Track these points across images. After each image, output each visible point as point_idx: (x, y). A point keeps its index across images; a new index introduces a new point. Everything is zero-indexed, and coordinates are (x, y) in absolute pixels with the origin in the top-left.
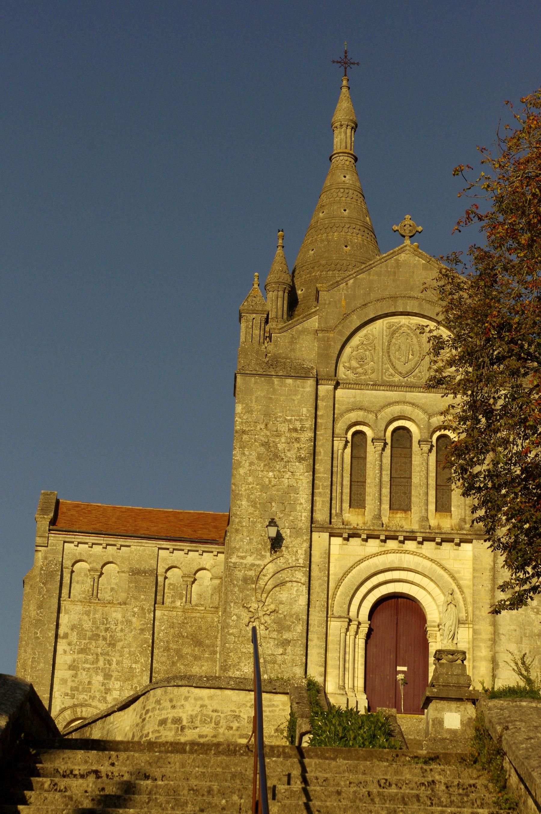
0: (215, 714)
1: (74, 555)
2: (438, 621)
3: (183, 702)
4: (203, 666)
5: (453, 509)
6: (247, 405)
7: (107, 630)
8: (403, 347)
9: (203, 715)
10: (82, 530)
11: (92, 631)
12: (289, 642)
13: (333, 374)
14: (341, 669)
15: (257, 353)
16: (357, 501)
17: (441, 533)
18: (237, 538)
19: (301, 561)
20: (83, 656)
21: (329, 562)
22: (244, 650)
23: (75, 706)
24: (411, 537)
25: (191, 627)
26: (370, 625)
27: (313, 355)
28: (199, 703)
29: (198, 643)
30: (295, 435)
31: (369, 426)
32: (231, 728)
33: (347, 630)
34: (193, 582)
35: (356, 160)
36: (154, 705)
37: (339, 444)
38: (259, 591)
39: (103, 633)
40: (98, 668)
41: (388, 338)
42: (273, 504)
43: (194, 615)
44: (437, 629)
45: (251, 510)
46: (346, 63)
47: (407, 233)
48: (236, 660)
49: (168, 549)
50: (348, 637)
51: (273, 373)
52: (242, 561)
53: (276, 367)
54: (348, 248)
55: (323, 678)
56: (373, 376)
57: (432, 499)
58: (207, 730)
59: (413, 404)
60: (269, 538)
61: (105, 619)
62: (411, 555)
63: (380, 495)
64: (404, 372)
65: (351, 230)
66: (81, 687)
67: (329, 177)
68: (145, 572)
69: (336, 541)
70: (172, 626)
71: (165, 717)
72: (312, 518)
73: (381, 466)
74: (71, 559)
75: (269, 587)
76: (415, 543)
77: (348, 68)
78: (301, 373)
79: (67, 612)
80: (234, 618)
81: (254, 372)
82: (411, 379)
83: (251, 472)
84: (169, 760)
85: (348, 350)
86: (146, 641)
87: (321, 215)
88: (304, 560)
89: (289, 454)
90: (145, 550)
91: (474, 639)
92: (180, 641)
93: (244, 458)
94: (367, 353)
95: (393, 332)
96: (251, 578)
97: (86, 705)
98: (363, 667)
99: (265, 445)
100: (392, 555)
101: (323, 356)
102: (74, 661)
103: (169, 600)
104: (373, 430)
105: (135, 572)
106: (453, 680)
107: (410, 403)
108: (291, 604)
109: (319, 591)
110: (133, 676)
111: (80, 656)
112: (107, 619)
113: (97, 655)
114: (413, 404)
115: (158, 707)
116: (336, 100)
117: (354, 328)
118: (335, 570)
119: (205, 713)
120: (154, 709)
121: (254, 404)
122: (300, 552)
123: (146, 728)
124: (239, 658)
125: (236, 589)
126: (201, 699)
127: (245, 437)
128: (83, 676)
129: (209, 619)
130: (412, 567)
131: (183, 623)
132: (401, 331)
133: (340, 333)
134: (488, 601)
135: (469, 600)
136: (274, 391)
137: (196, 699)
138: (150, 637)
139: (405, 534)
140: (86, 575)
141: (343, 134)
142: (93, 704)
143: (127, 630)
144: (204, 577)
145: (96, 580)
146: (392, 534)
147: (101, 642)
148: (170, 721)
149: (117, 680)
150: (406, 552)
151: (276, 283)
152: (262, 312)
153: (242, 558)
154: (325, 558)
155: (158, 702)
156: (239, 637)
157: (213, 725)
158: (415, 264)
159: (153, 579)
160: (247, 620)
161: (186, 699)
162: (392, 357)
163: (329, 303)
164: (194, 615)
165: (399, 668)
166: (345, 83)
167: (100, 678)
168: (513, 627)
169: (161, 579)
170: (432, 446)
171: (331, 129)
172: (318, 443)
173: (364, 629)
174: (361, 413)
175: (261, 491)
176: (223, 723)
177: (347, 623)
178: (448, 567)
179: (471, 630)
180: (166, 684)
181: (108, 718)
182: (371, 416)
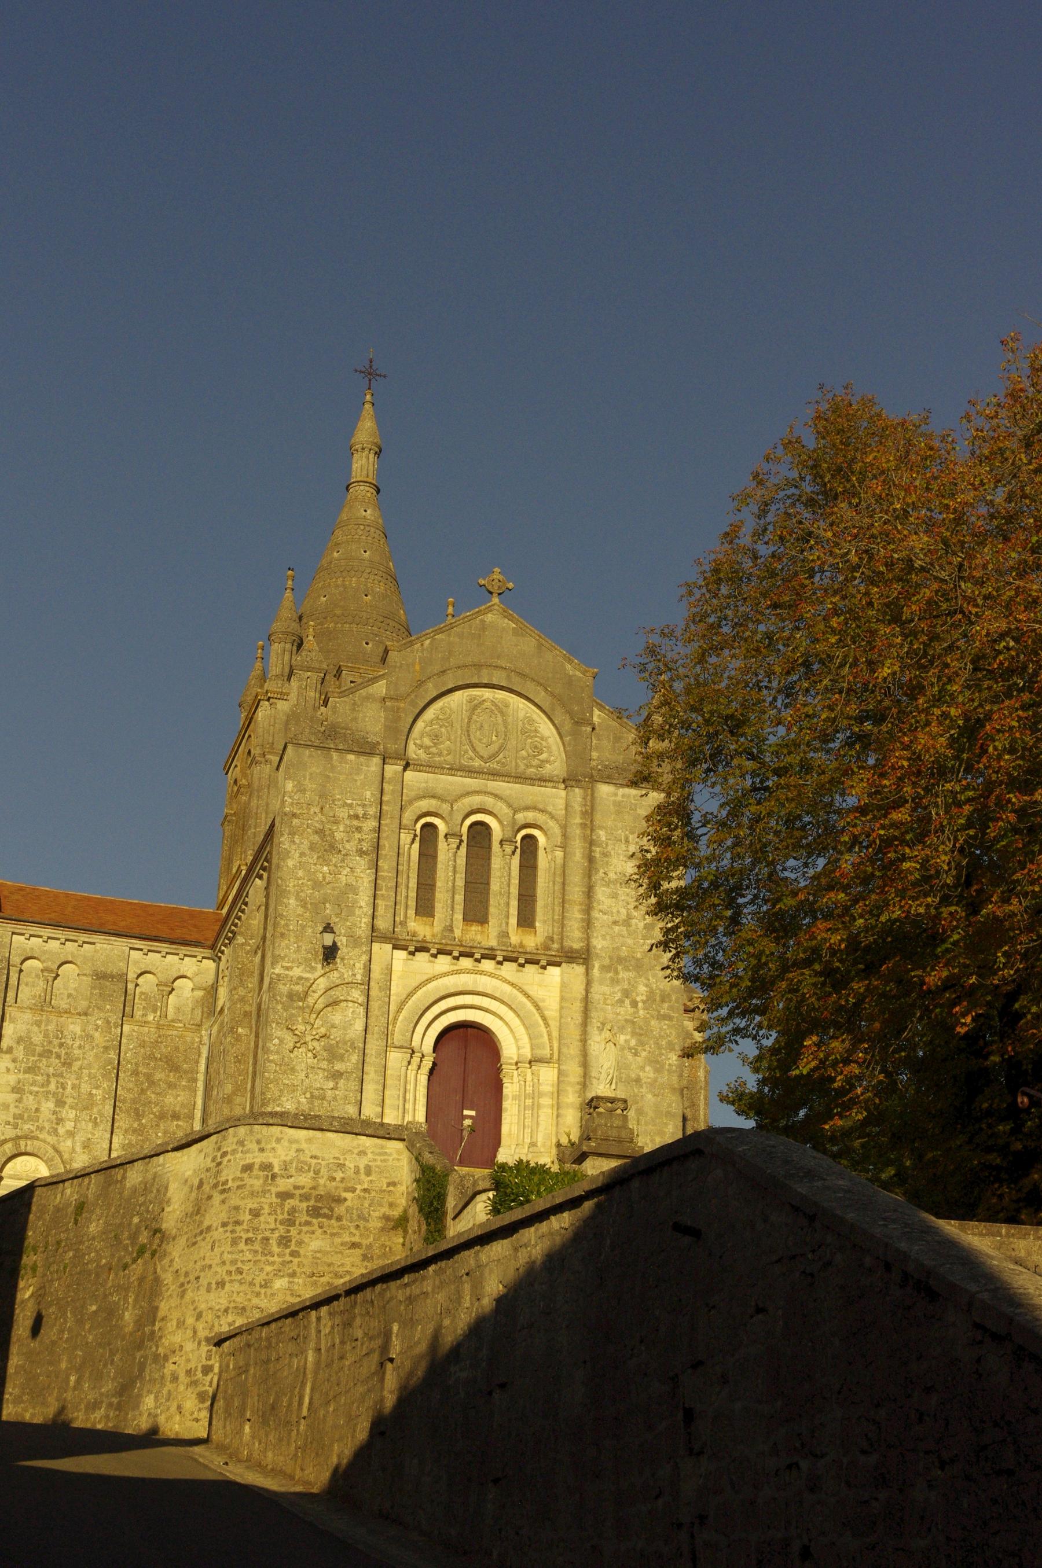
0: (314, 1161)
1: (25, 950)
2: (516, 1059)
3: (274, 1145)
4: (179, 1095)
5: (537, 924)
6: (299, 782)
7: (61, 1045)
8: (486, 727)
9: (299, 1161)
10: (35, 920)
11: (43, 1046)
12: (342, 1074)
14: (401, 1110)
15: (311, 720)
16: (425, 907)
17: (526, 953)
18: (283, 944)
19: (359, 977)
20: (31, 1076)
22: (287, 1082)
23: (18, 1137)
25: (166, 1047)
27: (378, 728)
28: (295, 1146)
29: (174, 1068)
30: (355, 823)
32: (334, 1179)
33: (409, 1063)
34: (170, 993)
35: (378, 491)
36: (234, 1147)
37: (406, 837)
38: (307, 1010)
39: (57, 1050)
40: (49, 1092)
41: (468, 714)
42: (328, 905)
43: (170, 1033)
44: (514, 1067)
45: (300, 911)
46: (370, 373)
47: (495, 589)
48: (277, 1094)
49: (141, 950)
50: (409, 1072)
51: (332, 746)
52: (287, 972)
53: (334, 739)
54: (369, 597)
56: (449, 758)
57: (514, 911)
58: (304, 1180)
59: (496, 796)
60: (323, 946)
61: (60, 1031)
62: (488, 977)
63: (453, 902)
65: (372, 577)
66: (26, 1115)
67: (346, 510)
68: (112, 977)
69: (400, 955)
70: (143, 1045)
71: (251, 1161)
73: (455, 867)
74: (20, 955)
76: (493, 962)
77: (373, 381)
78: (366, 749)
80: (276, 1041)
81: (309, 743)
82: (493, 765)
83: (301, 865)
84: (1012, 1246)
85: (420, 724)
87: (335, 554)
88: (363, 976)
89: (348, 846)
90: (113, 950)
91: (559, 1082)
92: (152, 1064)
93: (294, 847)
94: (443, 730)
95: (475, 706)
96: (298, 993)
97: (33, 1138)
98: (425, 1109)
99: (320, 832)
100: (465, 975)
101: (391, 729)
102: (19, 1082)
103: (140, 1013)
104: (447, 823)
105: (100, 976)
106: (613, 1133)
107: (492, 794)
108: (345, 1029)
109: (379, 1014)
110: (92, 1104)
111: (27, 1076)
112: (62, 1033)
113: (48, 1075)
114: (496, 796)
115: (241, 1149)
118: (397, 989)
119: (302, 1159)
120: (234, 1151)
121: (307, 782)
122: (357, 965)
123: (224, 1173)
125: (279, 1007)
126: (297, 1141)
127: (295, 821)
128: (30, 1101)
129: (188, 1039)
130: (489, 992)
131: (157, 1042)
132: (484, 707)
133: (413, 703)
134: (578, 1037)
136: (333, 767)
137: (291, 1142)
139: (483, 951)
140: (37, 976)
141: (364, 460)
142: (41, 1136)
143: (87, 1047)
145: (50, 983)
146: (468, 950)
147: (54, 1060)
148: (257, 1167)
149: (72, 1108)
150: (482, 973)
151: (283, 633)
152: (319, 670)
154: (386, 974)
155: (241, 1143)
156: (281, 1065)
157: (312, 1174)
158: (503, 628)
159: (122, 985)
160: (292, 1045)
161: (278, 1140)
162: (472, 737)
163: (401, 667)
164: (170, 1033)
165: (466, 1112)
166: (368, 397)
167: (51, 1105)
169: (131, 986)
170: (516, 847)
171: (350, 452)
172: (383, 835)
173: (428, 1064)
174: (434, 802)
175: (313, 889)
176: (324, 1172)
178: (531, 993)
179: (556, 1070)
180: (251, 1121)
181: (155, 1158)
182: (446, 807)
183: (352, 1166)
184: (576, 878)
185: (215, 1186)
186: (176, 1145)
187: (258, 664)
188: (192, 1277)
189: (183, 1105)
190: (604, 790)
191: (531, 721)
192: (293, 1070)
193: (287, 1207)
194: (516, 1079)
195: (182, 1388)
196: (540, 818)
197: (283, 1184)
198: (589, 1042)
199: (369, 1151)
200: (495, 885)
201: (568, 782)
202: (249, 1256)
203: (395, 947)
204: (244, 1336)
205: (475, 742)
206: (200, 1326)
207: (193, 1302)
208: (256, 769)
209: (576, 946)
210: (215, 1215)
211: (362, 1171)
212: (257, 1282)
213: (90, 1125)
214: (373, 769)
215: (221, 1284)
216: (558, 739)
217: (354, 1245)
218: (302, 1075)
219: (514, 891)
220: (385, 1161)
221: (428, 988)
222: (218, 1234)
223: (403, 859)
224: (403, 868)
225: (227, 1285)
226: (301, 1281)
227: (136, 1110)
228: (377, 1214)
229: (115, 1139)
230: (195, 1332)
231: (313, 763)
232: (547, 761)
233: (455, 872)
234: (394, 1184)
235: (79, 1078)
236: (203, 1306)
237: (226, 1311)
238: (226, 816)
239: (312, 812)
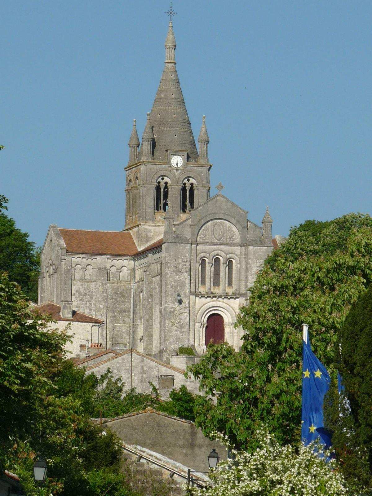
7: (89, 292)
16: (203, 282)
29: (123, 296)
30: (184, 263)
37: (198, 264)
39: (88, 293)
45: (171, 289)
57: (227, 282)
59: (221, 250)
61: (89, 288)
62: (220, 303)
64: (218, 239)
69: (197, 298)
75: (178, 314)
78: (186, 242)
79: (74, 285)
82: (221, 241)
83: (171, 277)
86: (104, 296)
99: (175, 267)
101: (193, 234)
105: (99, 269)
114: (221, 250)
127: (169, 264)
140: (80, 270)
141: (171, 53)
144: (124, 269)
149: (94, 311)
167: (88, 311)
169: (108, 271)
173: (206, 325)
174: (205, 254)
178: (231, 305)
182: (208, 255)
184: (243, 273)
189: (127, 308)
190: (251, 248)
191: (230, 227)
192: (172, 332)
196: (233, 256)
200: (222, 275)
201: (241, 245)
203: (196, 296)
209: (243, 292)
213: (100, 316)
219: (227, 277)
221: (203, 306)
223: (197, 271)
224: (197, 273)
227: (113, 310)
232: (235, 239)
235: (96, 301)
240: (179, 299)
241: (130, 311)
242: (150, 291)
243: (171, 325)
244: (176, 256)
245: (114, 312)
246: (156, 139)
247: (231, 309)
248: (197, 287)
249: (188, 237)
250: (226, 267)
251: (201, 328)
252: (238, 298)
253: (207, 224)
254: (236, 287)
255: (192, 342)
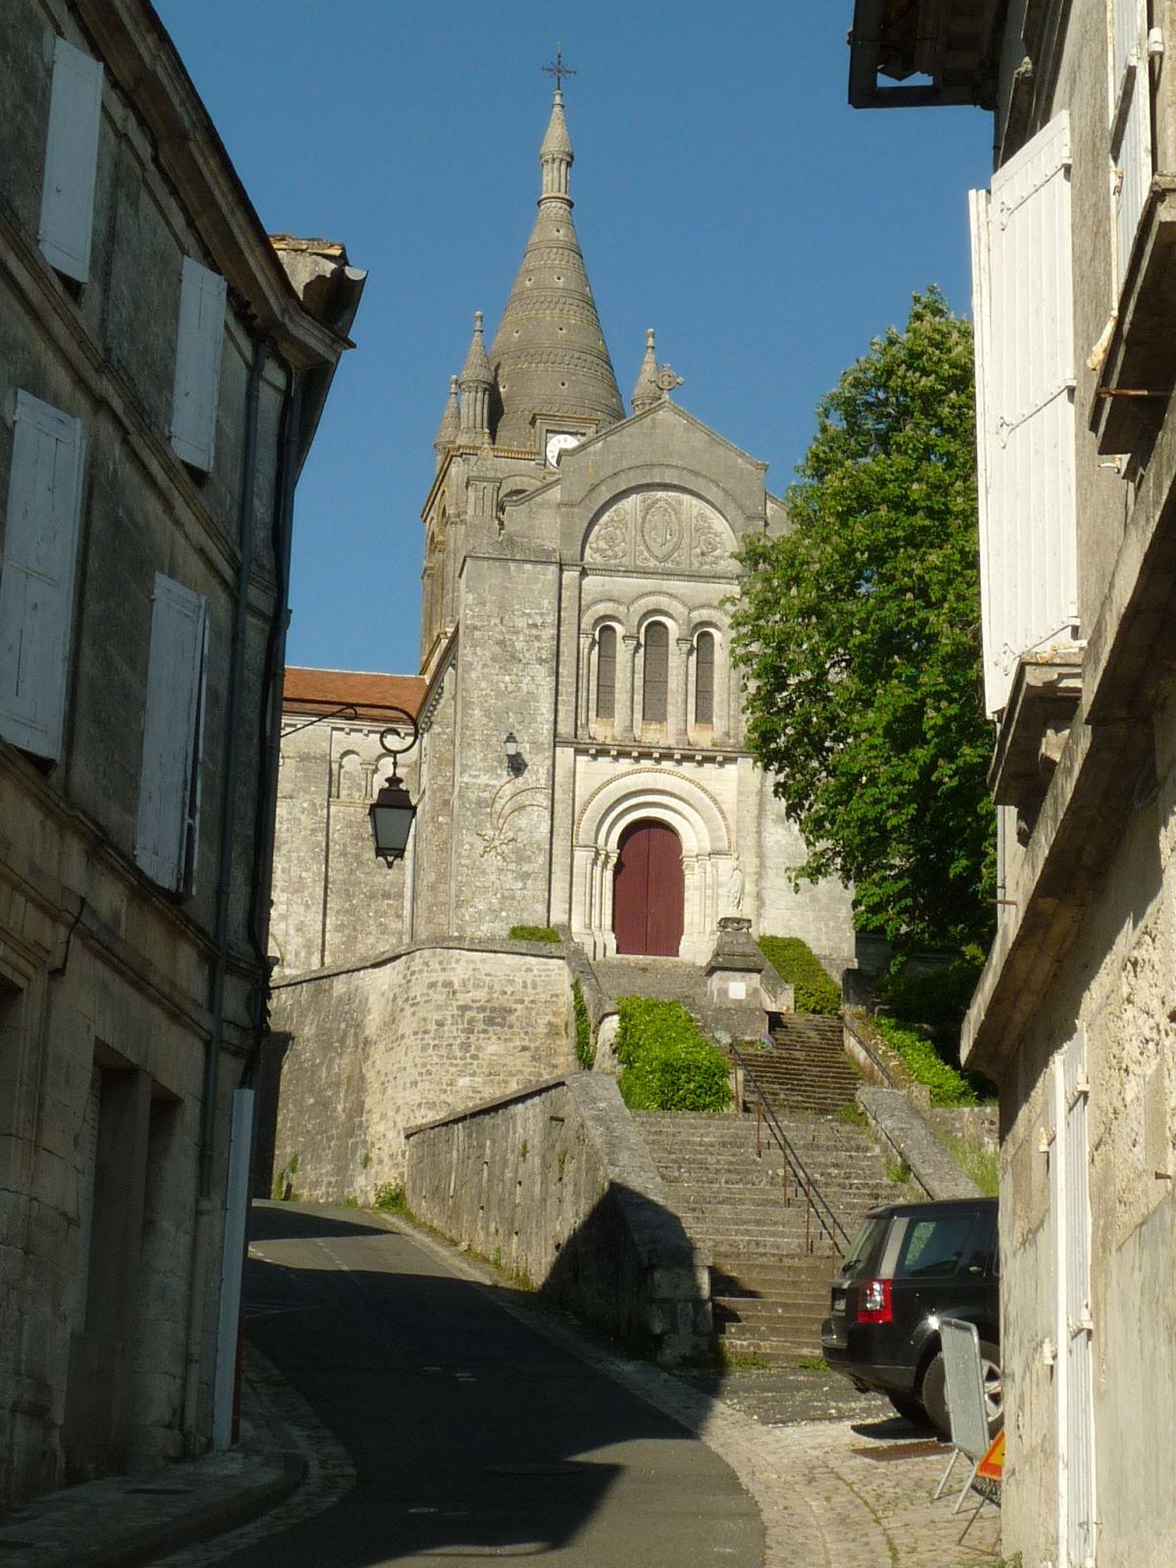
0: (488, 978)
3: (453, 965)
5: (714, 719)
9: (476, 979)
13: (579, 558)
14: (588, 906)
16: (605, 708)
18: (469, 754)
19: (543, 781)
21: (574, 782)
24: (667, 756)
26: (620, 855)
28: (471, 966)
30: (534, 632)
31: (619, 621)
32: (505, 993)
35: (571, 204)
37: (585, 642)
45: (485, 721)
46: (559, 71)
47: (666, 386)
48: (470, 895)
49: (342, 729)
54: (564, 331)
55: (567, 916)
57: (692, 708)
58: (481, 995)
59: (671, 595)
64: (660, 556)
68: (315, 758)
72: (555, 730)
75: (507, 811)
78: (542, 559)
80: (467, 846)
81: (487, 555)
83: (484, 676)
86: (318, 844)
93: (476, 659)
94: (618, 532)
99: (502, 643)
100: (647, 775)
101: (566, 536)
108: (531, 832)
114: (671, 595)
116: (545, 123)
117: (602, 503)
120: (421, 971)
122: (541, 770)
124: (474, 893)
125: (469, 813)
126: (473, 962)
127: (477, 634)
130: (668, 789)
135: (733, 827)
137: (467, 962)
138: (324, 839)
146: (646, 750)
149: (282, 891)
153: (475, 777)
155: (427, 964)
159: (326, 766)
161: (457, 961)
166: (558, 99)
168: (781, 860)
169: (335, 766)
171: (539, 163)
172: (562, 642)
174: (610, 605)
176: (497, 987)
177: (593, 854)
178: (709, 788)
181: (356, 973)
182: (623, 609)
183: (520, 981)
185: (407, 1000)
186: (373, 962)
187: (452, 400)
188: (391, 1078)
189: (392, 884)
192: (484, 873)
193: (466, 1018)
194: (696, 870)
195: (386, 1169)
197: (463, 999)
198: (764, 834)
199: (535, 969)
200: (674, 682)
202: (436, 1059)
203: (578, 752)
204: (421, 1134)
205: (651, 543)
206: (399, 1118)
207: (392, 1098)
208: (451, 530)
210: (407, 1025)
211: (529, 986)
212: (444, 1080)
213: (302, 908)
214: (550, 577)
215: (415, 1084)
216: (732, 534)
217: (524, 1049)
218: (493, 878)
220: (548, 976)
222: (410, 1040)
224: (583, 671)
225: (419, 1084)
226: (480, 1079)
227: (347, 890)
228: (543, 1021)
229: (328, 922)
230: (395, 1123)
231: (492, 576)
233: (633, 673)
234: (557, 996)
235: (289, 861)
236: (400, 1102)
237: (419, 1105)
238: (426, 570)
239: (492, 624)
240: (512, 752)
241: (400, 896)
242: (441, 788)
243: (481, 850)
244: (503, 606)
245: (348, 895)
246: (503, 396)
247: (707, 800)
248: (582, 720)
249: (549, 545)
250: (690, 652)
251: (598, 869)
252: (733, 760)
253: (620, 505)
254: (724, 723)
255: (558, 917)
